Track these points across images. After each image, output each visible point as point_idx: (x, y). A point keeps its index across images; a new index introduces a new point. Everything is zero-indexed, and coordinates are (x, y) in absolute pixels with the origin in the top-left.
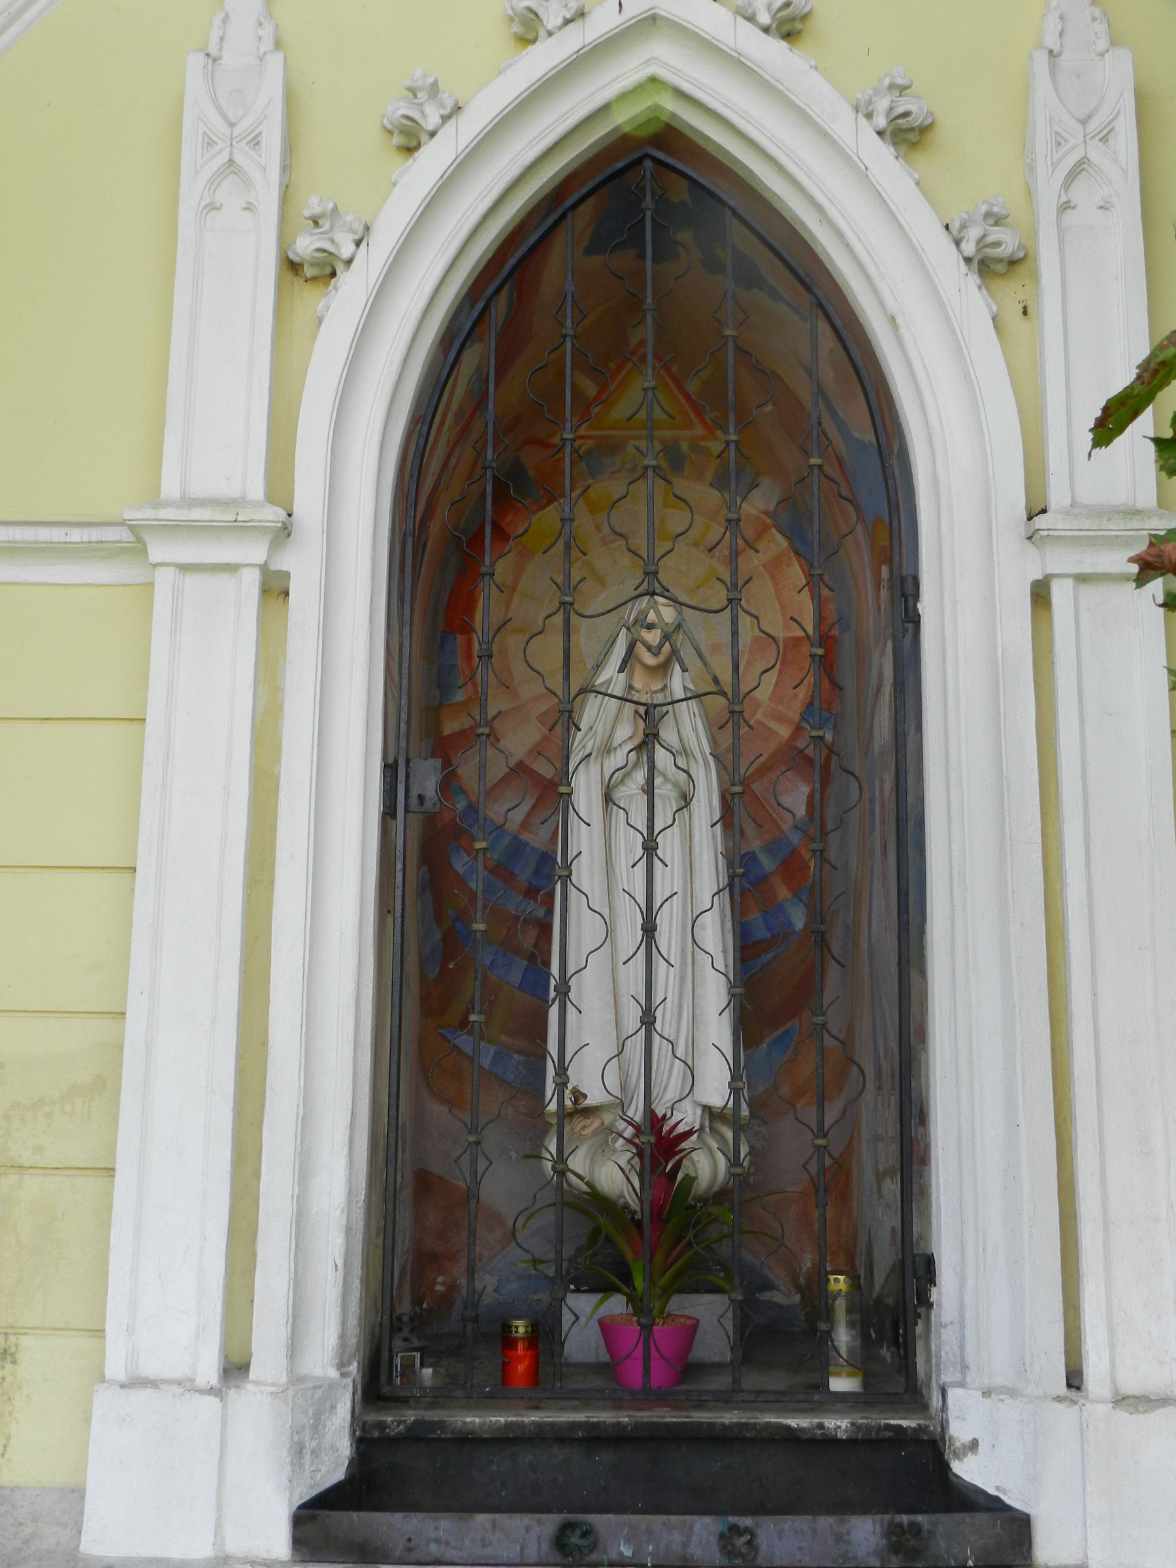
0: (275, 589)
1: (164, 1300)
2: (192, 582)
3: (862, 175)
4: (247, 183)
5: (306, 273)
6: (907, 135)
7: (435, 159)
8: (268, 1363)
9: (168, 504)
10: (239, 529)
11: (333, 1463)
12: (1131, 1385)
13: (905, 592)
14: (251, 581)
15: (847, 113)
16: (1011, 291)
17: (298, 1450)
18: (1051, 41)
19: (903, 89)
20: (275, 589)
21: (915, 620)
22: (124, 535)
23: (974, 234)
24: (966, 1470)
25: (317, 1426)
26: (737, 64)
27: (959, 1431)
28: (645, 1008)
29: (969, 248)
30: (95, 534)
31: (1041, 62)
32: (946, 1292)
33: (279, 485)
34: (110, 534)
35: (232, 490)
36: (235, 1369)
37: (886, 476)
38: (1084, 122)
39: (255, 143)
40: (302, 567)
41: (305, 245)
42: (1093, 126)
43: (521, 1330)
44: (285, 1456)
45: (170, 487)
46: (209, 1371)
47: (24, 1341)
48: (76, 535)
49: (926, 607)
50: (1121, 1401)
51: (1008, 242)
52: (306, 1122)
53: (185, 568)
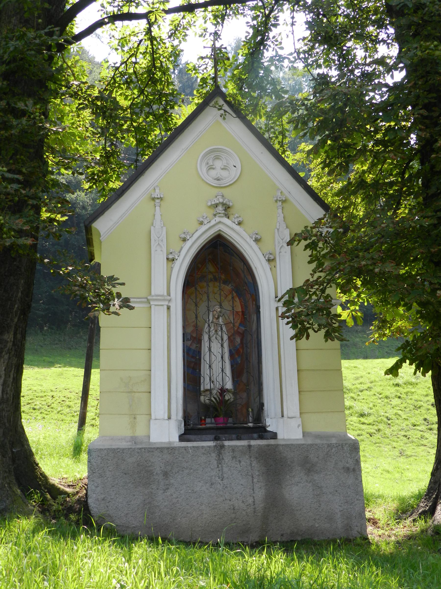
0: (169, 308)
1: (159, 407)
2: (157, 307)
3: (251, 247)
4: (161, 247)
5: (171, 260)
6: (257, 241)
7: (188, 244)
8: (173, 416)
9: (153, 296)
10: (164, 300)
11: (182, 431)
12: (290, 416)
13: (258, 308)
14: (165, 307)
15: (249, 237)
16: (273, 264)
17: (179, 428)
18: (278, 227)
19: (257, 234)
20: (169, 308)
21: (260, 312)
22: (146, 300)
23: (267, 256)
24: (268, 429)
25: (181, 426)
26: (233, 229)
27: (267, 424)
28: (217, 371)
29: (267, 258)
30: (141, 300)
31: (276, 230)
32: (265, 407)
33: (169, 294)
34: (143, 300)
35: (162, 294)
36: (169, 418)
37: (255, 290)
38: (282, 240)
39: (162, 241)
40: (172, 305)
41: (171, 257)
42: (284, 240)
43: (379, 137)
44: (177, 428)
45: (153, 293)
46: (166, 417)
47: (138, 416)
48: (138, 300)
49: (261, 310)
50: (288, 418)
51: (272, 257)
52: (177, 384)
53: (155, 305)
